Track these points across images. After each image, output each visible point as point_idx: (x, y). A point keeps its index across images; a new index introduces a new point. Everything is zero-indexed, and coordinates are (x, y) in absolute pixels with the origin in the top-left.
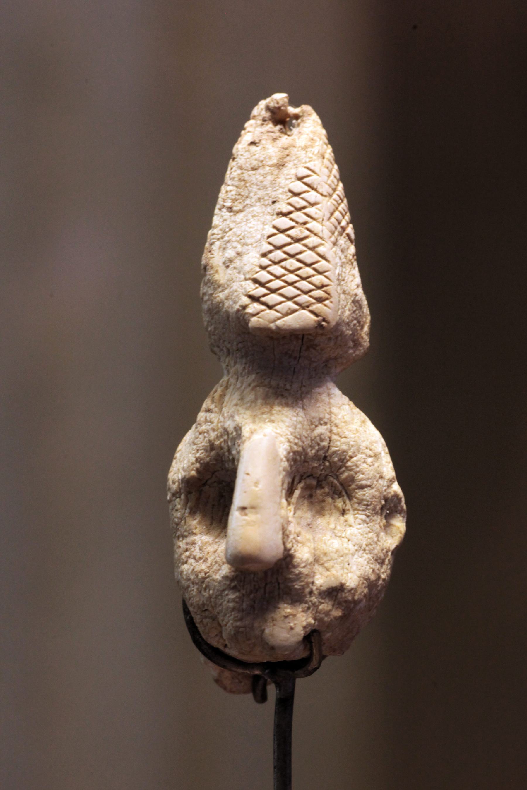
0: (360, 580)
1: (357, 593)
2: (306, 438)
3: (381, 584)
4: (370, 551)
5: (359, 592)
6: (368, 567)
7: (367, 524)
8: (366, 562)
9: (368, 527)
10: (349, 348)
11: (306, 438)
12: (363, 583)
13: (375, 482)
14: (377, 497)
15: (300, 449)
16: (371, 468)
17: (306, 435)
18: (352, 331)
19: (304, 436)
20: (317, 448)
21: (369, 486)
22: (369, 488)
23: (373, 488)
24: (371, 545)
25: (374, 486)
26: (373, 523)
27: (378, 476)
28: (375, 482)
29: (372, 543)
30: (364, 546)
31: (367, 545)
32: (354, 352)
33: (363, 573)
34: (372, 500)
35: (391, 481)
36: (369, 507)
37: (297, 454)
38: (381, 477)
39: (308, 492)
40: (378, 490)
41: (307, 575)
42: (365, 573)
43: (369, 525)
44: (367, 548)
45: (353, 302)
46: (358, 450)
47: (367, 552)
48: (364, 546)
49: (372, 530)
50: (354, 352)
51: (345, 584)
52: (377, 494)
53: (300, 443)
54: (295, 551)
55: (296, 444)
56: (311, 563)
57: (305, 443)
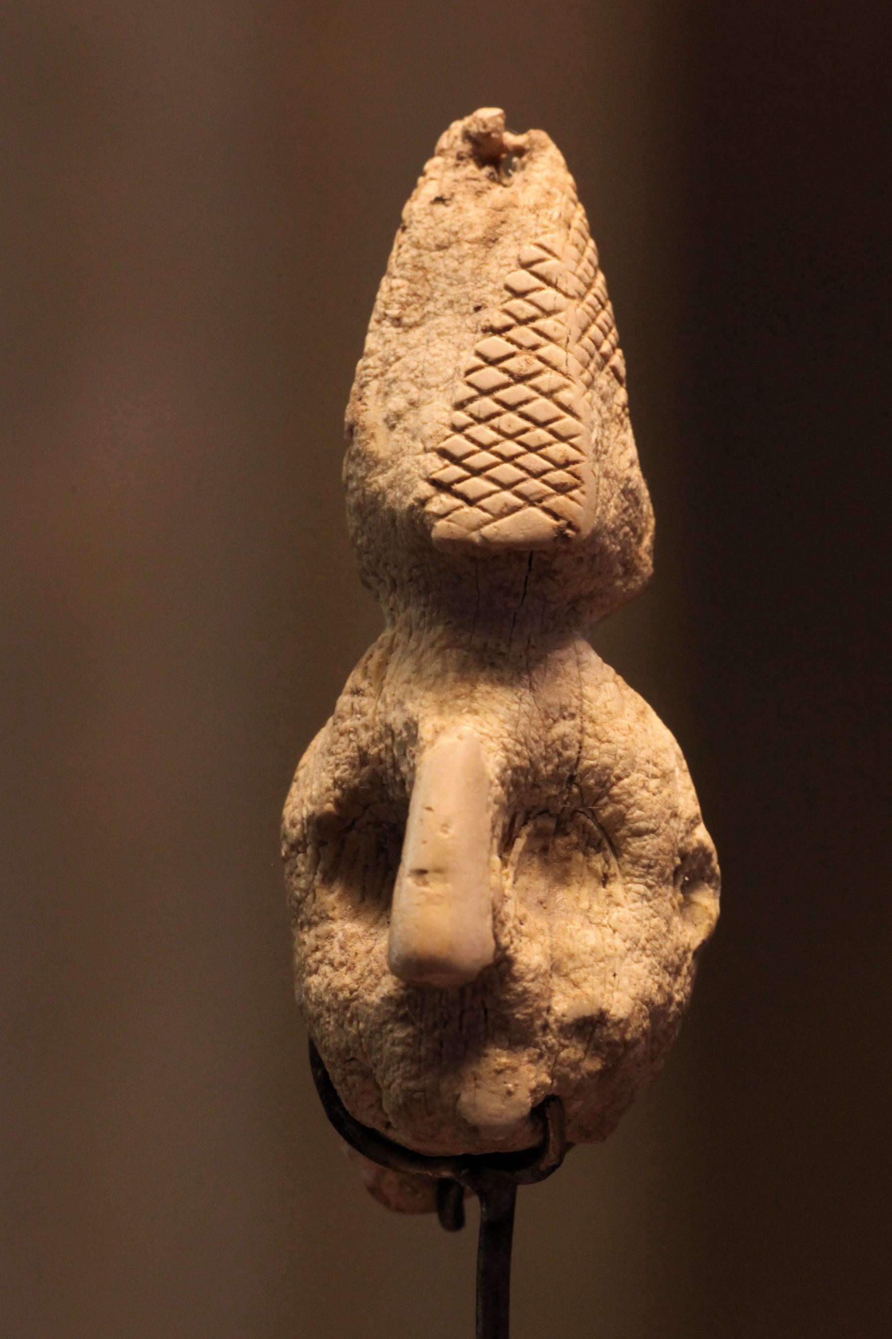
0: (636, 1005)
1: (630, 1029)
2: (536, 742)
3: (674, 1012)
4: (653, 950)
5: (633, 1026)
6: (650, 981)
8: (646, 972)
9: (651, 907)
11: (536, 742)
13: (663, 825)
14: (667, 852)
15: (526, 763)
16: (655, 798)
17: (537, 738)
19: (533, 738)
21: (653, 831)
22: (652, 835)
23: (659, 835)
24: (656, 940)
25: (661, 830)
26: (660, 899)
27: (669, 812)
28: (663, 825)
29: (657, 936)
31: (648, 940)
34: (657, 857)
35: (692, 822)
36: (651, 871)
39: (540, 843)
41: (537, 995)
43: (651, 903)
44: (648, 946)
47: (648, 952)
49: (658, 912)
52: (667, 846)
53: (526, 753)
54: (516, 951)
55: (518, 754)
57: (535, 752)
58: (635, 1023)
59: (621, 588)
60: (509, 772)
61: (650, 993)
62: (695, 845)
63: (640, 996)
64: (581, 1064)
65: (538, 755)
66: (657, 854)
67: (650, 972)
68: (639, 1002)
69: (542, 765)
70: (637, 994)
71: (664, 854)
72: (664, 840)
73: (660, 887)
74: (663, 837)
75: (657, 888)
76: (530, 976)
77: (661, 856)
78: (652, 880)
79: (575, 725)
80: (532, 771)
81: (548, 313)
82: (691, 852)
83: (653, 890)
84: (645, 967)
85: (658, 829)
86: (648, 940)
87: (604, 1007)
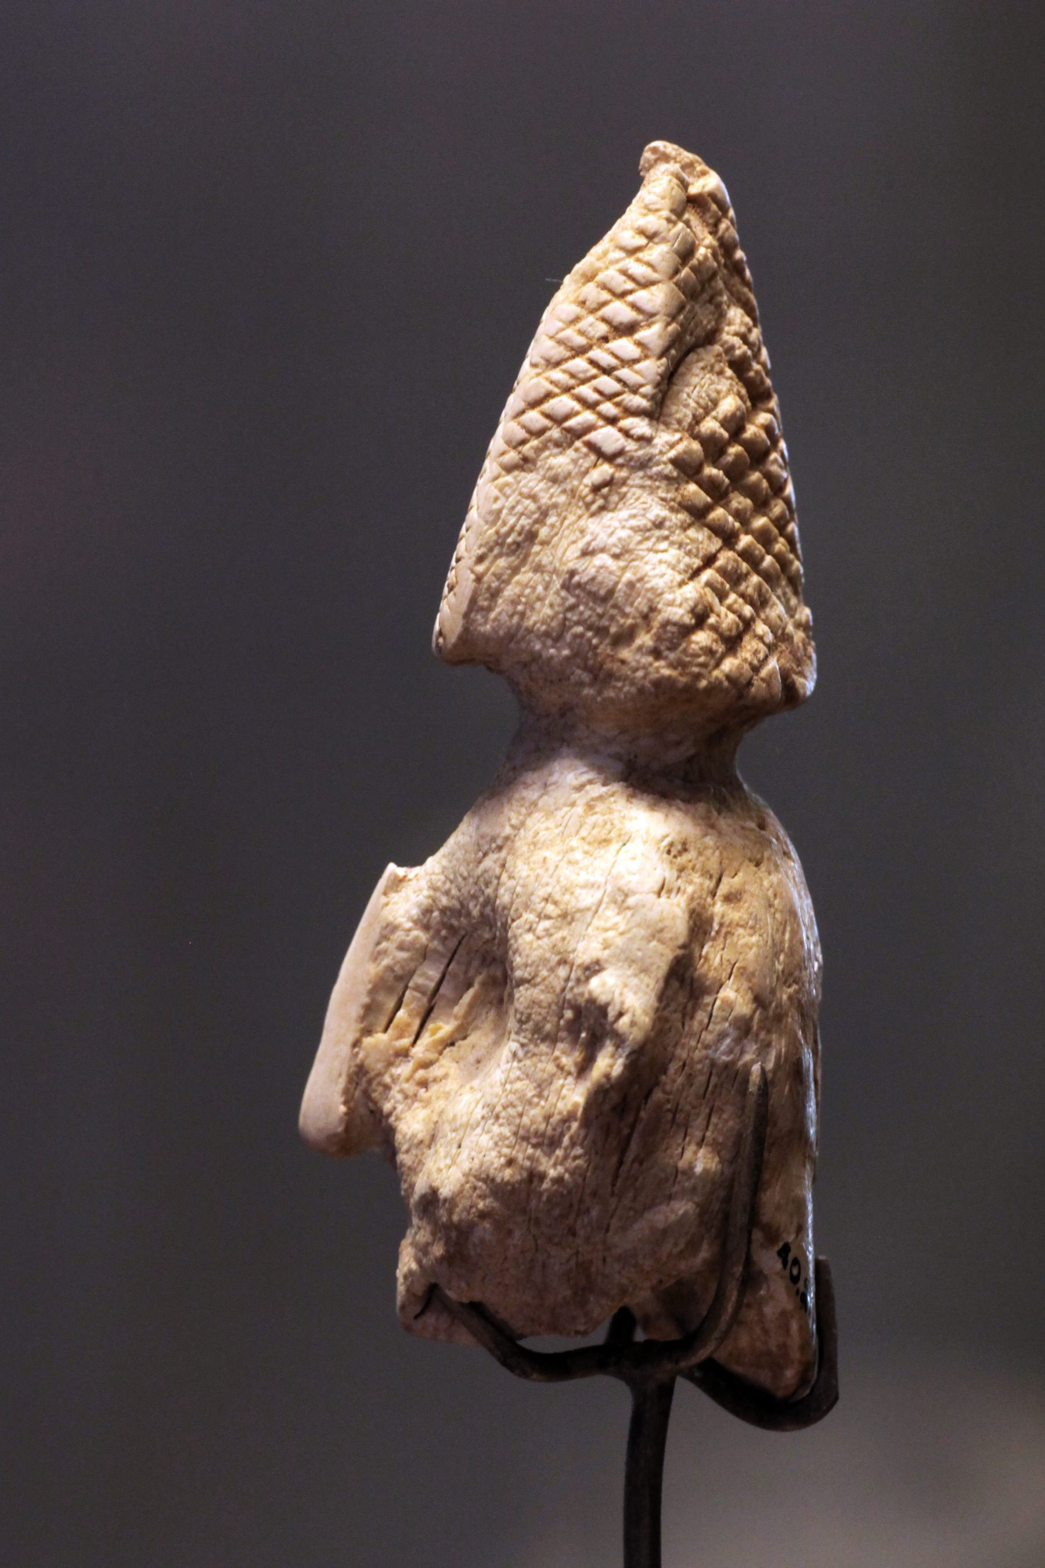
0: (467, 1182)
1: (457, 1210)
2: (465, 879)
3: (546, 1190)
4: (508, 1119)
5: (461, 1206)
6: (494, 1154)
7: (520, 1061)
8: (491, 1144)
9: (520, 1069)
10: (581, 684)
11: (465, 879)
12: (475, 1188)
13: (544, 973)
14: (545, 1004)
15: (456, 904)
16: (540, 942)
17: (466, 874)
18: (572, 650)
19: (461, 875)
20: (481, 899)
21: (528, 981)
22: (527, 985)
23: (535, 986)
24: (514, 1107)
25: (538, 980)
26: (535, 1059)
27: (555, 959)
28: (544, 973)
29: (517, 1102)
30: (499, 1108)
31: (505, 1108)
32: (600, 693)
33: (477, 1166)
34: (529, 1011)
35: (587, 968)
36: (524, 1027)
37: (448, 913)
38: (563, 962)
39: (493, 994)
40: (549, 989)
41: (409, 1168)
42: (481, 1165)
43: (522, 1064)
44: (503, 1114)
45: (566, 586)
46: (527, 907)
47: (501, 1121)
48: (499, 1108)
49: (527, 1075)
50: (600, 693)
51: (438, 1189)
52: (545, 998)
53: (454, 892)
54: (398, 1119)
55: (447, 893)
56: (421, 1142)
57: (463, 891)
58: (463, 1203)
59: (594, 698)
60: (436, 914)
61: (488, 1168)
62: (586, 996)
63: (473, 1171)
64: (429, 1248)
65: (466, 894)
66: (528, 1007)
67: (496, 1144)
68: (472, 1179)
69: (471, 905)
70: (471, 1169)
71: (540, 1007)
72: (542, 991)
73: (536, 1045)
74: (542, 987)
75: (531, 1047)
76: (405, 1147)
77: (536, 1009)
78: (525, 1037)
79: (498, 859)
80: (463, 912)
81: (584, 382)
82: (583, 1004)
83: (526, 1049)
84: (492, 1138)
85: (533, 978)
86: (505, 1108)
87: (434, 1184)
